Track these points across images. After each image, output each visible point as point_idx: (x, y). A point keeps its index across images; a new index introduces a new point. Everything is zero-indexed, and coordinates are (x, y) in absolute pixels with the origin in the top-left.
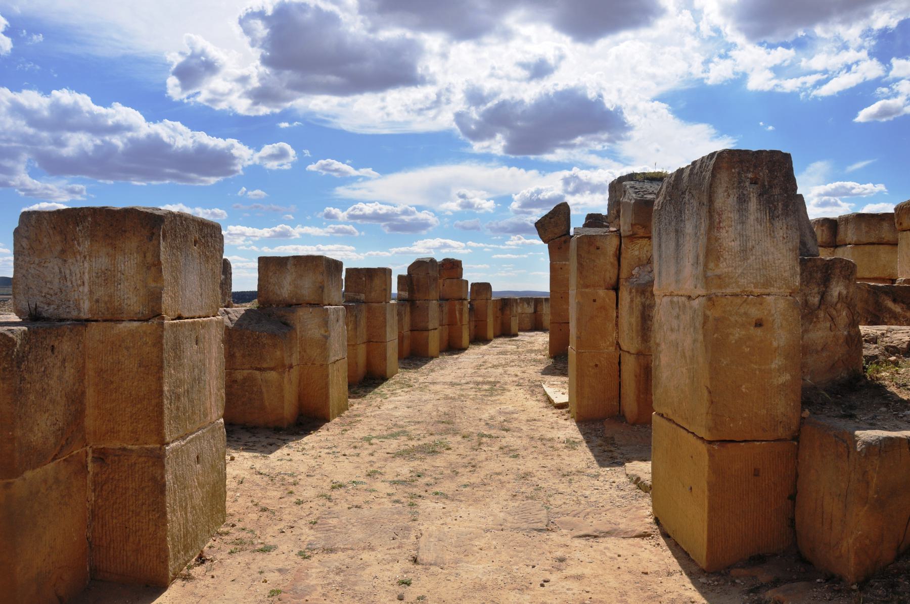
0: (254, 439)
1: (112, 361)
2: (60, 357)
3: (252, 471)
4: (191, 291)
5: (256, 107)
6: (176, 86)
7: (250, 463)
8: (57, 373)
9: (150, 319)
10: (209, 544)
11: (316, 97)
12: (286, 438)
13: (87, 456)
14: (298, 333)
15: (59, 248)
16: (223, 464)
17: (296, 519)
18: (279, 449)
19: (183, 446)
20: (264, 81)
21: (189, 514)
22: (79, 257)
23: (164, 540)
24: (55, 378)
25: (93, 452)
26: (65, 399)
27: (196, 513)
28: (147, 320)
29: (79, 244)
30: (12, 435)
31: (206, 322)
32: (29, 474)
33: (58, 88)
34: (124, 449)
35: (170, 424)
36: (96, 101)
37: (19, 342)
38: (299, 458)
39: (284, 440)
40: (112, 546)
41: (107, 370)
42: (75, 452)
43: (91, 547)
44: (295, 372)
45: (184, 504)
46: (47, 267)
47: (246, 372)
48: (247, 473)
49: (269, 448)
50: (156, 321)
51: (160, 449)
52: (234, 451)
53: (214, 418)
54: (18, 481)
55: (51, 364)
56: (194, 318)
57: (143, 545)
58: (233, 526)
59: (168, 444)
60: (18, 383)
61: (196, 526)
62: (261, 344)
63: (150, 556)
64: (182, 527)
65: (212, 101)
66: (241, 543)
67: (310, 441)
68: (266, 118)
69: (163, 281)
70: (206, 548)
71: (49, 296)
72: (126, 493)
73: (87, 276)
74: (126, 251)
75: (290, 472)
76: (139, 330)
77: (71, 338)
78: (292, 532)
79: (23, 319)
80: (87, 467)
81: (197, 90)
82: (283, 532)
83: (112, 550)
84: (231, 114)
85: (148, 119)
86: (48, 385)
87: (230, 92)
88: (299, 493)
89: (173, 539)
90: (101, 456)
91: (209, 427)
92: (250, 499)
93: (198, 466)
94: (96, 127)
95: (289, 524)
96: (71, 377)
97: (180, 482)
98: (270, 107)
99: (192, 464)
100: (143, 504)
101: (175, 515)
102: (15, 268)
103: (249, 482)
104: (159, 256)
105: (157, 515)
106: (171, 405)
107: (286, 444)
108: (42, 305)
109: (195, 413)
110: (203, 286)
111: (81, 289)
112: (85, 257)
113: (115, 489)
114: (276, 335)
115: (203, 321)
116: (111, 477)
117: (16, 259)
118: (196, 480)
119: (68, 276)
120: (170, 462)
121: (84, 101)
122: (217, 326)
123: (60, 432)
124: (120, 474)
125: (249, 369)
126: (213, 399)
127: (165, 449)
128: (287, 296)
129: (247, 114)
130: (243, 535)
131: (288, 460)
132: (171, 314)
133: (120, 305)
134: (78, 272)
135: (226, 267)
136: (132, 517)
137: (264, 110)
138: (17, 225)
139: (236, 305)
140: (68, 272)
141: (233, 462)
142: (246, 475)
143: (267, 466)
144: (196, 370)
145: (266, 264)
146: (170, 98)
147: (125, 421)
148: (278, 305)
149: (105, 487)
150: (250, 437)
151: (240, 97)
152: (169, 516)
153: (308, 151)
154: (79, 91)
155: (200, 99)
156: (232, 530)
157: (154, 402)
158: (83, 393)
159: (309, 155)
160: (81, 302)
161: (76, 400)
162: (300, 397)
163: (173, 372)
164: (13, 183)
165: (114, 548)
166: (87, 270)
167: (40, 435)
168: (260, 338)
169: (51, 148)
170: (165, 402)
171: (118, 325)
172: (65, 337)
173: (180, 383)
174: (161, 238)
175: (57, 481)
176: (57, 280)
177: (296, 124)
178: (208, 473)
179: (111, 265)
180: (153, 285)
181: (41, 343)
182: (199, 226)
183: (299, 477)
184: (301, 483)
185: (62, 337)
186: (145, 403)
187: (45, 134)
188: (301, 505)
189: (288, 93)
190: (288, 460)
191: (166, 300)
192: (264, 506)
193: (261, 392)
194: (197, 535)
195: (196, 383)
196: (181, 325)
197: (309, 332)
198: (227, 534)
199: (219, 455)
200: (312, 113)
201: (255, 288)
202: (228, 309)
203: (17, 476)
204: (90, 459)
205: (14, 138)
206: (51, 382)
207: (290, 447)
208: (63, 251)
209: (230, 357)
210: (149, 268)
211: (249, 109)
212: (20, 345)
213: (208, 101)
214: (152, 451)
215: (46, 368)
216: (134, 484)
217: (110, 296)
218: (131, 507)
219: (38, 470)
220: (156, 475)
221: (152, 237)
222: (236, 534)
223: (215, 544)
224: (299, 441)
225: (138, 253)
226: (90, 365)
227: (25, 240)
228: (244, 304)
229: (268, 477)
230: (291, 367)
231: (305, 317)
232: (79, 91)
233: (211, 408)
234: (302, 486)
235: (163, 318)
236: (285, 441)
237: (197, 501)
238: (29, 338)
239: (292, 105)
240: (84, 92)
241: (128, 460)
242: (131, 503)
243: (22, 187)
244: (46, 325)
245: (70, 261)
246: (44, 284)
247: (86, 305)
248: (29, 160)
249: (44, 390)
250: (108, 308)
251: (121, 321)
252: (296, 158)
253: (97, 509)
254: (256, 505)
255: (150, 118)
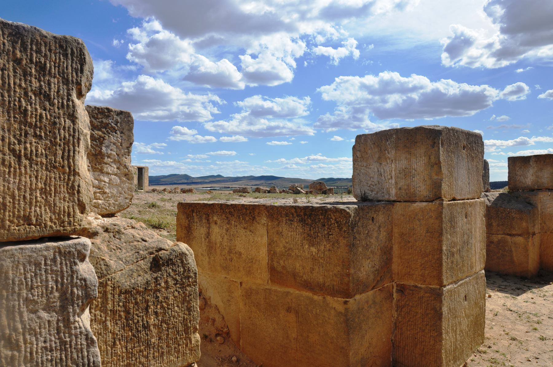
0: (505, 283)
1: (409, 228)
2: (377, 225)
3: (504, 307)
4: (462, 181)
5: (499, 62)
6: (447, 58)
7: (503, 301)
8: (375, 234)
9: (433, 200)
10: (471, 358)
11: (542, 47)
12: (530, 285)
13: (393, 288)
14: (539, 210)
15: (377, 156)
16: (484, 302)
17: (541, 352)
18: (525, 293)
19: (456, 288)
20: (504, 44)
21: (458, 336)
22: (388, 161)
23: (440, 352)
24: (374, 238)
25: (397, 286)
26: (380, 251)
27: (463, 335)
28: (432, 201)
29: (388, 153)
30: (349, 272)
31: (473, 203)
32: (358, 297)
33: (382, 71)
34: (416, 287)
35: (447, 272)
36: (402, 75)
37: (353, 215)
38: (541, 302)
39: (529, 287)
40: (406, 348)
41: (406, 234)
42: (386, 285)
43: (394, 346)
44: (537, 239)
45: (455, 329)
46: (371, 168)
47: (500, 237)
48: (500, 309)
49: (518, 291)
50: (438, 202)
51: (440, 289)
52: (491, 291)
53: (478, 270)
54: (351, 300)
55: (372, 229)
56: (464, 200)
57: (426, 352)
58: (489, 347)
59: (445, 286)
60: (352, 240)
61: (463, 344)
62: (511, 217)
63: (430, 360)
64: (452, 344)
65: (470, 63)
66: (495, 362)
67: (550, 289)
68: (507, 68)
69: (442, 174)
70: (469, 361)
71: (372, 186)
72: (416, 316)
73: (393, 173)
74: (418, 155)
75: (534, 313)
76: (427, 208)
77: (384, 213)
78: (537, 362)
79: (358, 200)
80: (393, 295)
81: (460, 58)
82: (530, 361)
83: (406, 350)
84: (483, 70)
85: (432, 81)
86: (370, 242)
87: (482, 55)
88: (542, 331)
89: (446, 352)
90: (402, 289)
91: (474, 276)
92: (503, 329)
93: (466, 302)
94: (403, 90)
95: (534, 355)
96: (384, 238)
97: (452, 313)
98: (509, 60)
99: (461, 301)
100: (427, 325)
101: (448, 335)
102: (353, 169)
103: (502, 315)
104: (439, 158)
105: (436, 334)
106: (447, 260)
107: (530, 290)
108: (368, 192)
109: (464, 266)
110: (470, 178)
111: (390, 181)
112: (392, 161)
113: (409, 311)
114: (522, 211)
115: (470, 202)
116: (407, 303)
117: (354, 164)
118: (463, 312)
119: (382, 173)
120: (446, 299)
121: (396, 76)
122: (480, 205)
123: (377, 272)
124: (413, 303)
125: (502, 234)
126: (477, 256)
127: (443, 290)
128: (530, 184)
129: (493, 67)
130: (497, 356)
131: (532, 303)
132: (448, 197)
133: (414, 191)
134: (388, 171)
135: (486, 165)
136: (420, 332)
137: (505, 63)
138: (354, 144)
139: (493, 190)
140: (382, 171)
141: (490, 299)
142: (499, 309)
143: (516, 305)
144: (466, 236)
145: (513, 162)
146: (444, 66)
147: (417, 268)
148: (523, 190)
149: (403, 310)
150: (502, 282)
151: (488, 57)
152: (444, 336)
153: (538, 86)
154: (393, 71)
155: (462, 63)
156: (489, 351)
157: (436, 257)
158: (391, 248)
159: (540, 88)
160: (391, 189)
161: (387, 252)
162: (541, 256)
163: (449, 237)
164: (362, 126)
165: (407, 350)
166: (394, 169)
167: (365, 273)
168: (510, 213)
169: (380, 104)
170: (444, 257)
171: (414, 204)
172: (380, 212)
173: (454, 245)
174: (440, 145)
175: (374, 302)
176: (376, 176)
177: (528, 68)
178: (473, 308)
179: (408, 165)
180: (436, 177)
181: (366, 215)
182: (466, 136)
183: (542, 318)
184: (544, 322)
185: (379, 212)
186: (430, 257)
187: (377, 98)
188: (545, 341)
189: (522, 48)
190: (532, 303)
191: (445, 187)
192: (514, 336)
193: (511, 251)
194: (463, 351)
195: (465, 244)
196: (455, 205)
197: (548, 209)
198: (485, 352)
199: (481, 295)
200: (541, 59)
201: (506, 179)
202: (487, 193)
203: (351, 298)
204: (394, 290)
205: (362, 102)
206: (372, 241)
207: (534, 293)
208: (379, 158)
209: (489, 226)
210: (432, 166)
211: (494, 65)
212: (354, 217)
213: (467, 63)
214: (434, 290)
215: (368, 231)
216: (421, 310)
217: (408, 186)
218: (419, 325)
219: (363, 295)
220: (436, 307)
221: (434, 145)
222: (491, 354)
223: (476, 358)
224: (541, 289)
225: (425, 156)
226: (396, 230)
227: (358, 152)
228: (498, 190)
229: (516, 314)
230: (534, 234)
231: (545, 198)
232: (393, 71)
233: (475, 263)
234: (545, 325)
235: (443, 200)
236: (530, 288)
237: (464, 327)
238: (359, 213)
239: (525, 56)
240: (395, 71)
241: (418, 294)
242: (419, 322)
243: (367, 128)
244: (369, 204)
245: (384, 163)
246: (369, 179)
247: (393, 191)
248: (370, 113)
249: (367, 245)
250: (407, 193)
251: (415, 202)
252: (530, 91)
253: (398, 323)
254: (507, 334)
255: (432, 80)
